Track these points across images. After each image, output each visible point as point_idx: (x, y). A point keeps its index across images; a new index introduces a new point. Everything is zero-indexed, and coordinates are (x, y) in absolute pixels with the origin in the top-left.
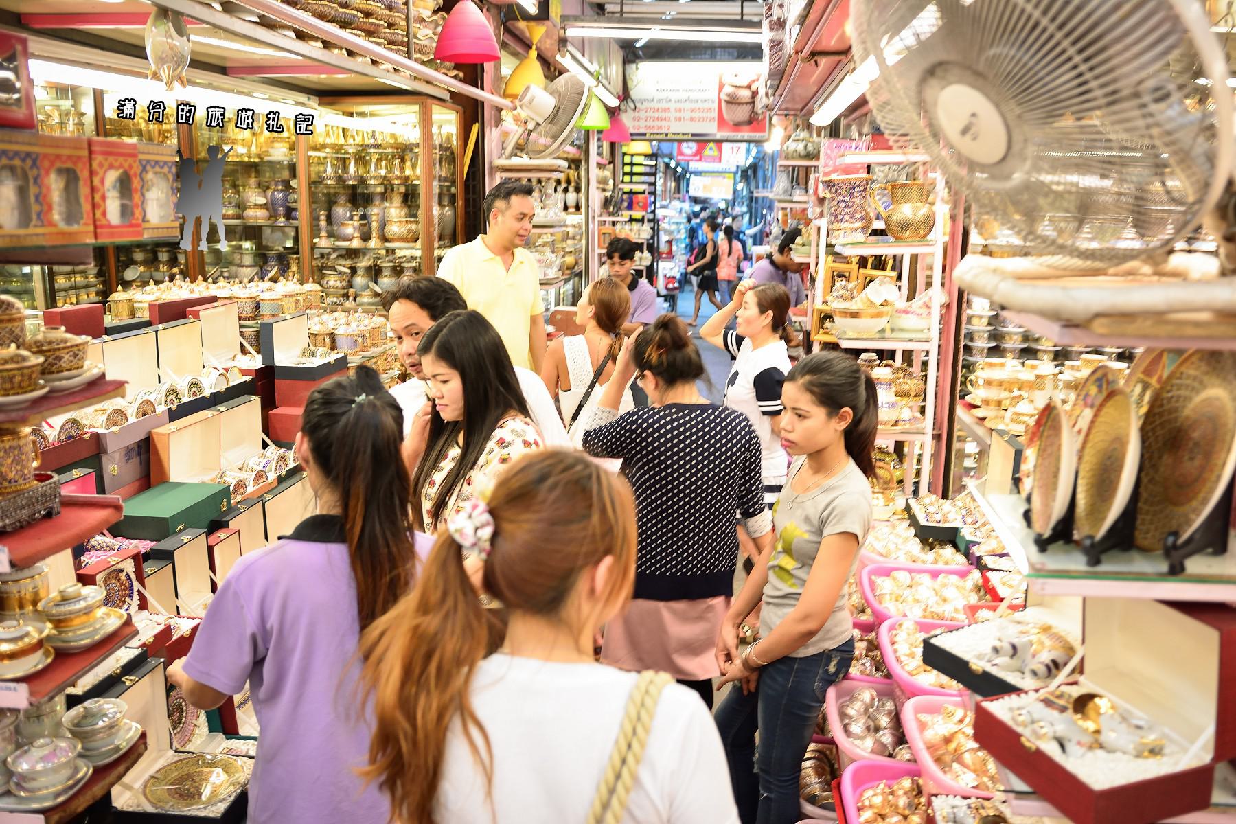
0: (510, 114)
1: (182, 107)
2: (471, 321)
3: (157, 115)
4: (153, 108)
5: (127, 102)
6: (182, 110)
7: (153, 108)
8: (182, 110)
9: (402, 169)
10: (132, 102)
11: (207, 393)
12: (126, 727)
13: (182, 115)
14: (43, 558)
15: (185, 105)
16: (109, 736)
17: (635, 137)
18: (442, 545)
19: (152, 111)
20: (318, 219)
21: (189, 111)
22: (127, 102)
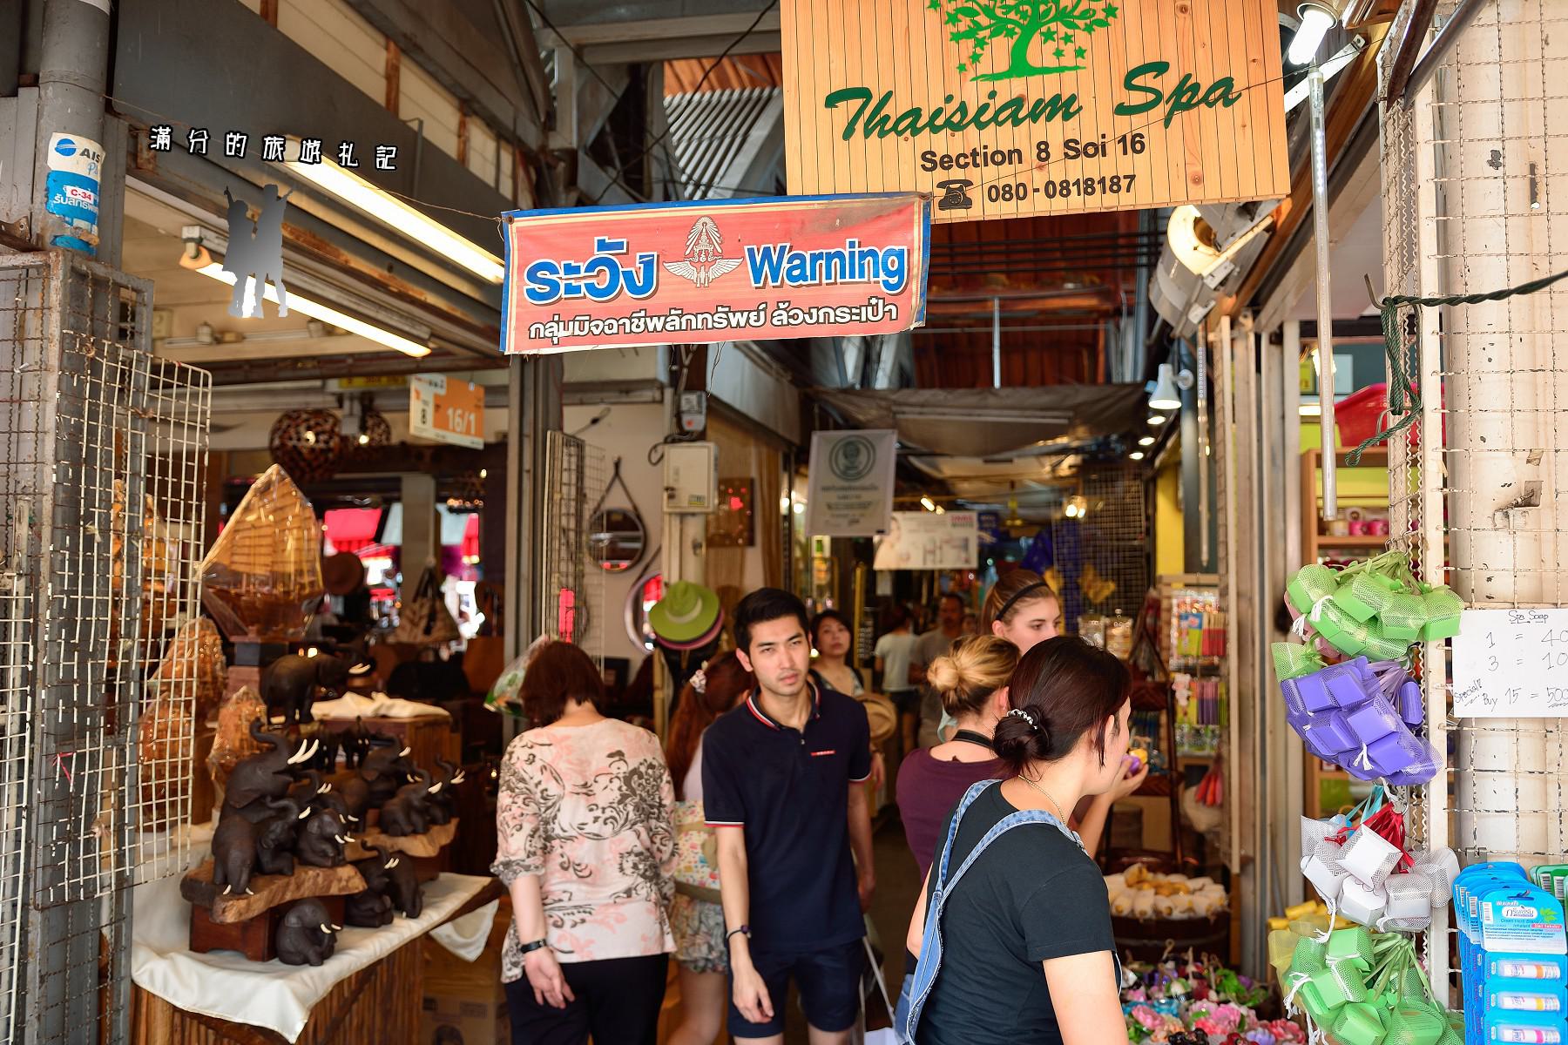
0: (257, 437)
1: (231, 135)
2: (1369, 529)
3: (198, 146)
4: (194, 137)
5: (161, 129)
6: (231, 140)
7: (194, 137)
8: (231, 140)
9: (1142, 246)
10: (168, 130)
11: (1180, 309)
12: (866, 496)
13: (231, 146)
14: (335, 508)
15: (235, 134)
16: (492, 608)
17: (519, 70)
18: (1046, 760)
19: (193, 141)
20: (350, 375)
21: (240, 141)
22: (161, 129)
